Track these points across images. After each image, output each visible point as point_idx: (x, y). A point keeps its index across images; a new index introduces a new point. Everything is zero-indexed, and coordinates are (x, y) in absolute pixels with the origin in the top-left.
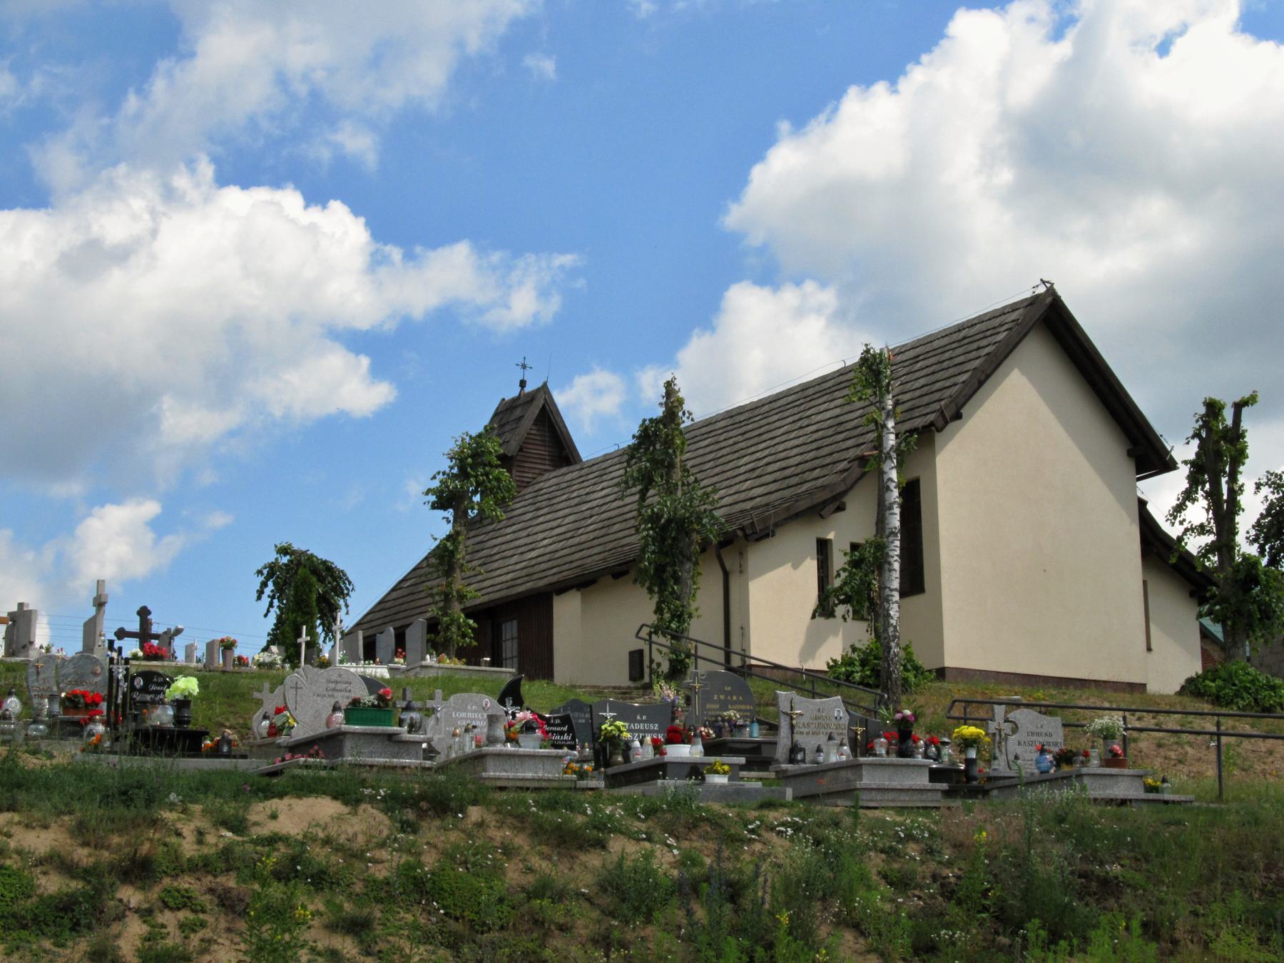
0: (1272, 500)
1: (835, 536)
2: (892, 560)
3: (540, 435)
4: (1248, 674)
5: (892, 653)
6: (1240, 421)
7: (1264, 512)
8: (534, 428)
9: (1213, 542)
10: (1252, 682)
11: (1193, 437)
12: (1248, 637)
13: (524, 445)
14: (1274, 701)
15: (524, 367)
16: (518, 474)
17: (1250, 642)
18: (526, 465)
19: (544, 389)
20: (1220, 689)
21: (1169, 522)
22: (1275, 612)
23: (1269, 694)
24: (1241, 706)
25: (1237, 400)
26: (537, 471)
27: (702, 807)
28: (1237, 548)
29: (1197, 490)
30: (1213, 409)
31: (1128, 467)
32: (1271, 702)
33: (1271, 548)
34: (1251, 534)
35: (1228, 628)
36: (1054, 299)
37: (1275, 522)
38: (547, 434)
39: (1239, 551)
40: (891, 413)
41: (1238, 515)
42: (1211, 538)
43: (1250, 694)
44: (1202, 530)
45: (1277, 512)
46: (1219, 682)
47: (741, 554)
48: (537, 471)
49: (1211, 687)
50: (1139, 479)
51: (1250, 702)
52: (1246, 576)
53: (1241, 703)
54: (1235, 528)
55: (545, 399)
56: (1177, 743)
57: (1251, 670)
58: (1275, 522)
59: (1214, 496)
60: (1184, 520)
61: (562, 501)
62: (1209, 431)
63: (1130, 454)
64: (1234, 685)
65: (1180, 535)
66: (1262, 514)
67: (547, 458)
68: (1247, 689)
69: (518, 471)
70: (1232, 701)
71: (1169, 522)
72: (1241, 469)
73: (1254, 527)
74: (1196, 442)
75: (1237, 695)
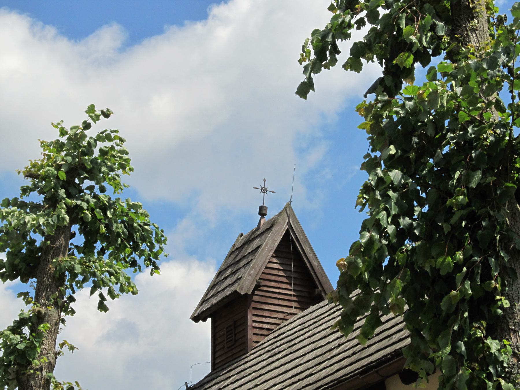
3: (283, 270)
8: (275, 260)
15: (264, 190)
16: (255, 318)
26: (281, 316)
27: (13, 206)
48: (281, 316)
55: (289, 223)
61: (305, 339)
65: (375, 98)
67: (293, 293)
69: (254, 315)
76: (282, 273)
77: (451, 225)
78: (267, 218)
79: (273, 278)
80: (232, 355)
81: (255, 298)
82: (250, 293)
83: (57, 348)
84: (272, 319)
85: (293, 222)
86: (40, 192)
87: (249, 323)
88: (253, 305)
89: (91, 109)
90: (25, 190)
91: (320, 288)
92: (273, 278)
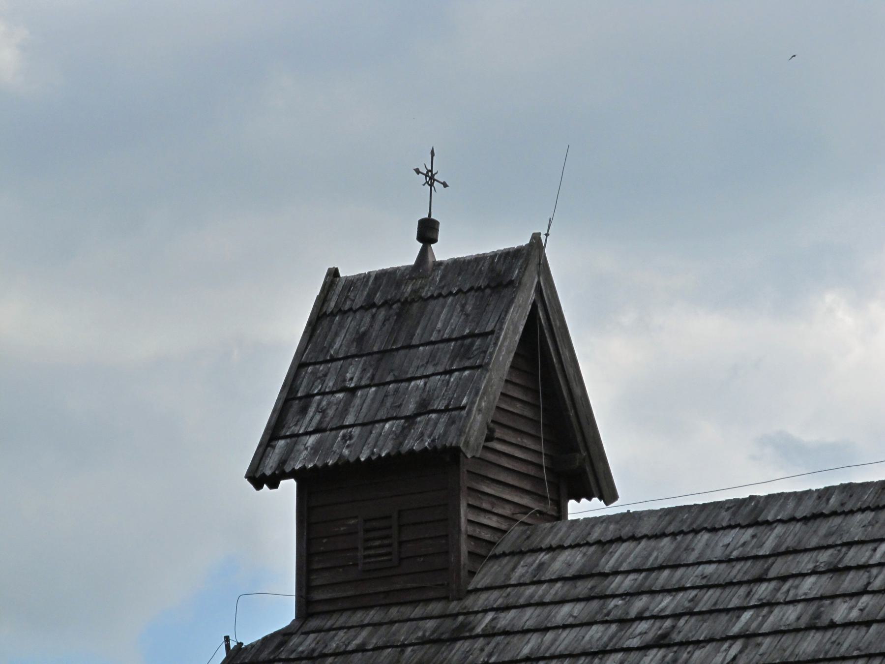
48: (507, 511)
77: (424, 254)
80: (387, 593)
84: (495, 518)
85: (545, 284)
91: (582, 451)
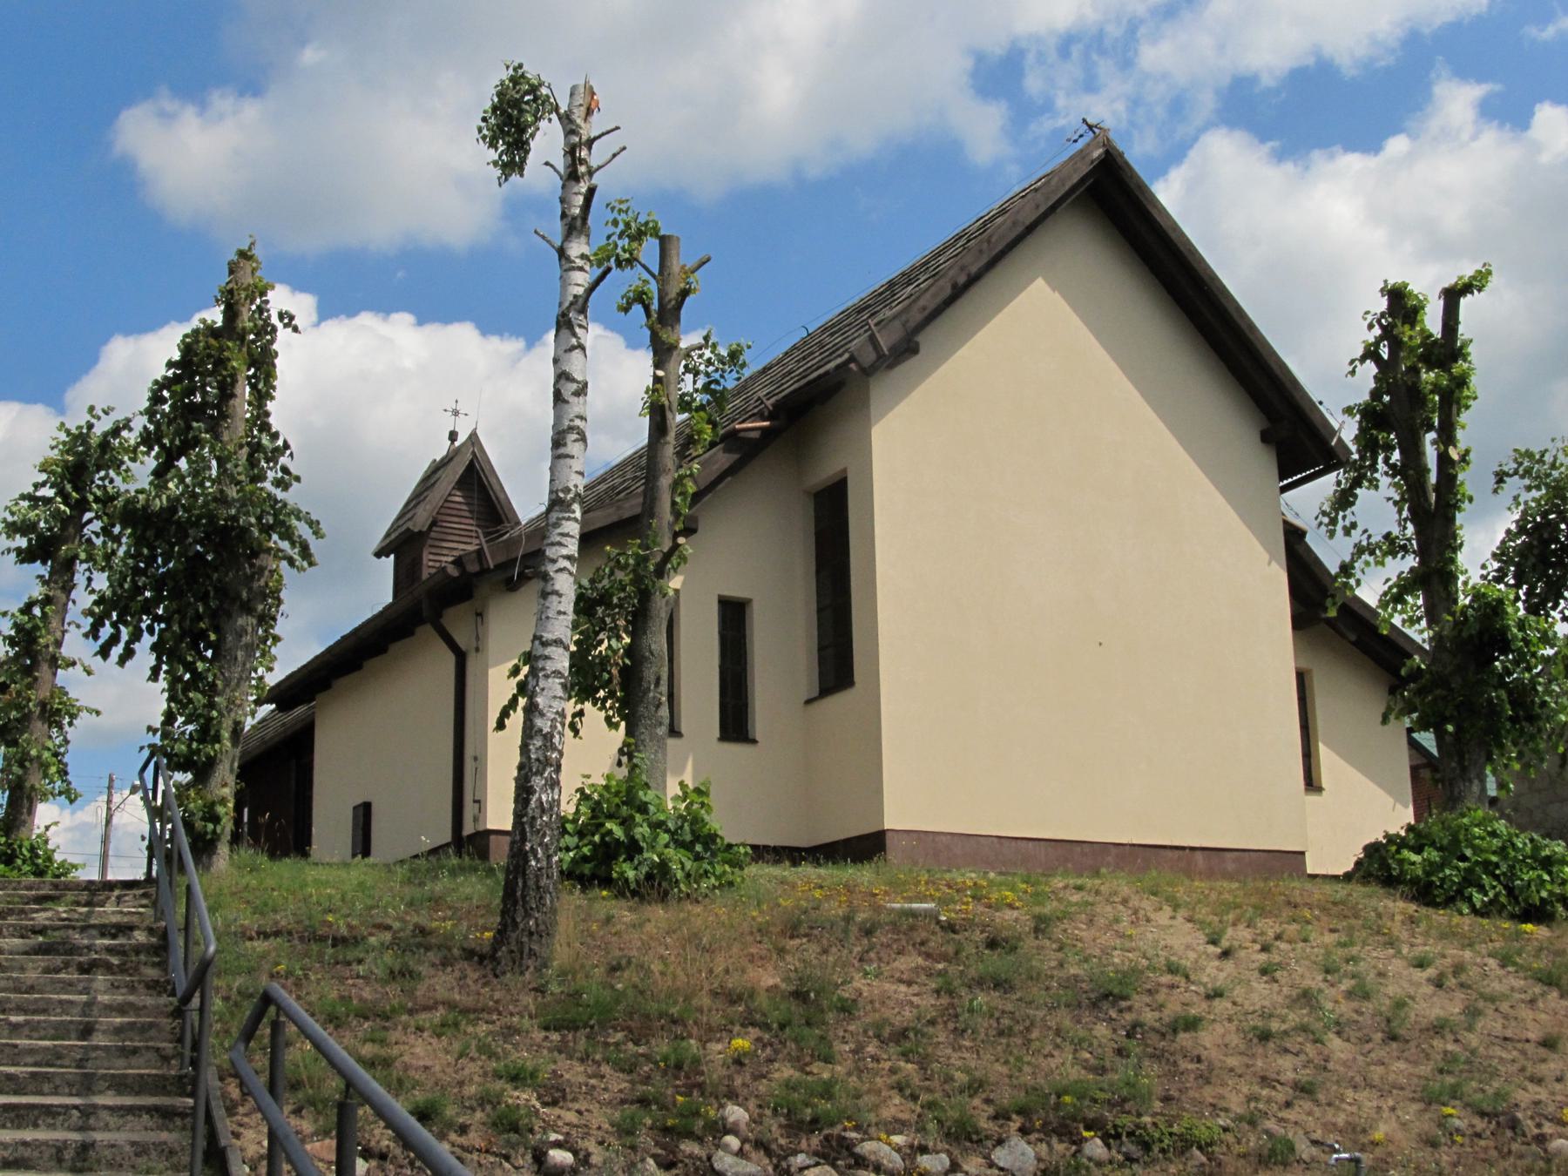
0: (1526, 503)
1: (684, 583)
2: (551, 568)
4: (1494, 834)
5: (533, 804)
6: (1457, 322)
7: (1513, 527)
9: (1412, 570)
10: (1502, 852)
11: (1363, 359)
12: (1489, 759)
13: (440, 517)
14: (1551, 893)
17: (1494, 772)
18: (445, 544)
19: (473, 438)
20: (1432, 868)
21: (1323, 528)
22: (1544, 704)
23: (1539, 877)
24: (1478, 905)
25: (1449, 282)
28: (1462, 578)
29: (1375, 462)
30: (1401, 304)
31: (1263, 464)
32: (1544, 894)
33: (1528, 594)
34: (1490, 569)
35: (1448, 739)
36: (1107, 152)
37: (1535, 543)
38: (476, 502)
39: (1465, 583)
40: (579, 223)
41: (1459, 509)
42: (1411, 561)
43: (1497, 877)
44: (1393, 546)
45: (1537, 526)
46: (1433, 855)
47: (480, 615)
49: (1413, 863)
50: (1284, 489)
51: (1497, 895)
52: (1481, 633)
53: (1478, 898)
54: (1455, 536)
55: (474, 453)
56: (1304, 1029)
57: (1501, 826)
58: (1535, 543)
59: (1410, 472)
60: (1354, 525)
62: (1396, 345)
63: (1266, 437)
64: (1463, 858)
66: (1508, 532)
68: (1489, 867)
70: (1460, 892)
71: (1323, 528)
72: (1464, 417)
73: (1494, 555)
74: (1371, 368)
75: (1470, 879)
76: (465, 507)
78: (457, 444)
79: (454, 512)
81: (433, 535)
82: (425, 529)
83: (66, 627)
86: (51, 487)
87: (425, 561)
88: (430, 542)
89: (91, 409)
90: (37, 486)
92: (454, 512)
